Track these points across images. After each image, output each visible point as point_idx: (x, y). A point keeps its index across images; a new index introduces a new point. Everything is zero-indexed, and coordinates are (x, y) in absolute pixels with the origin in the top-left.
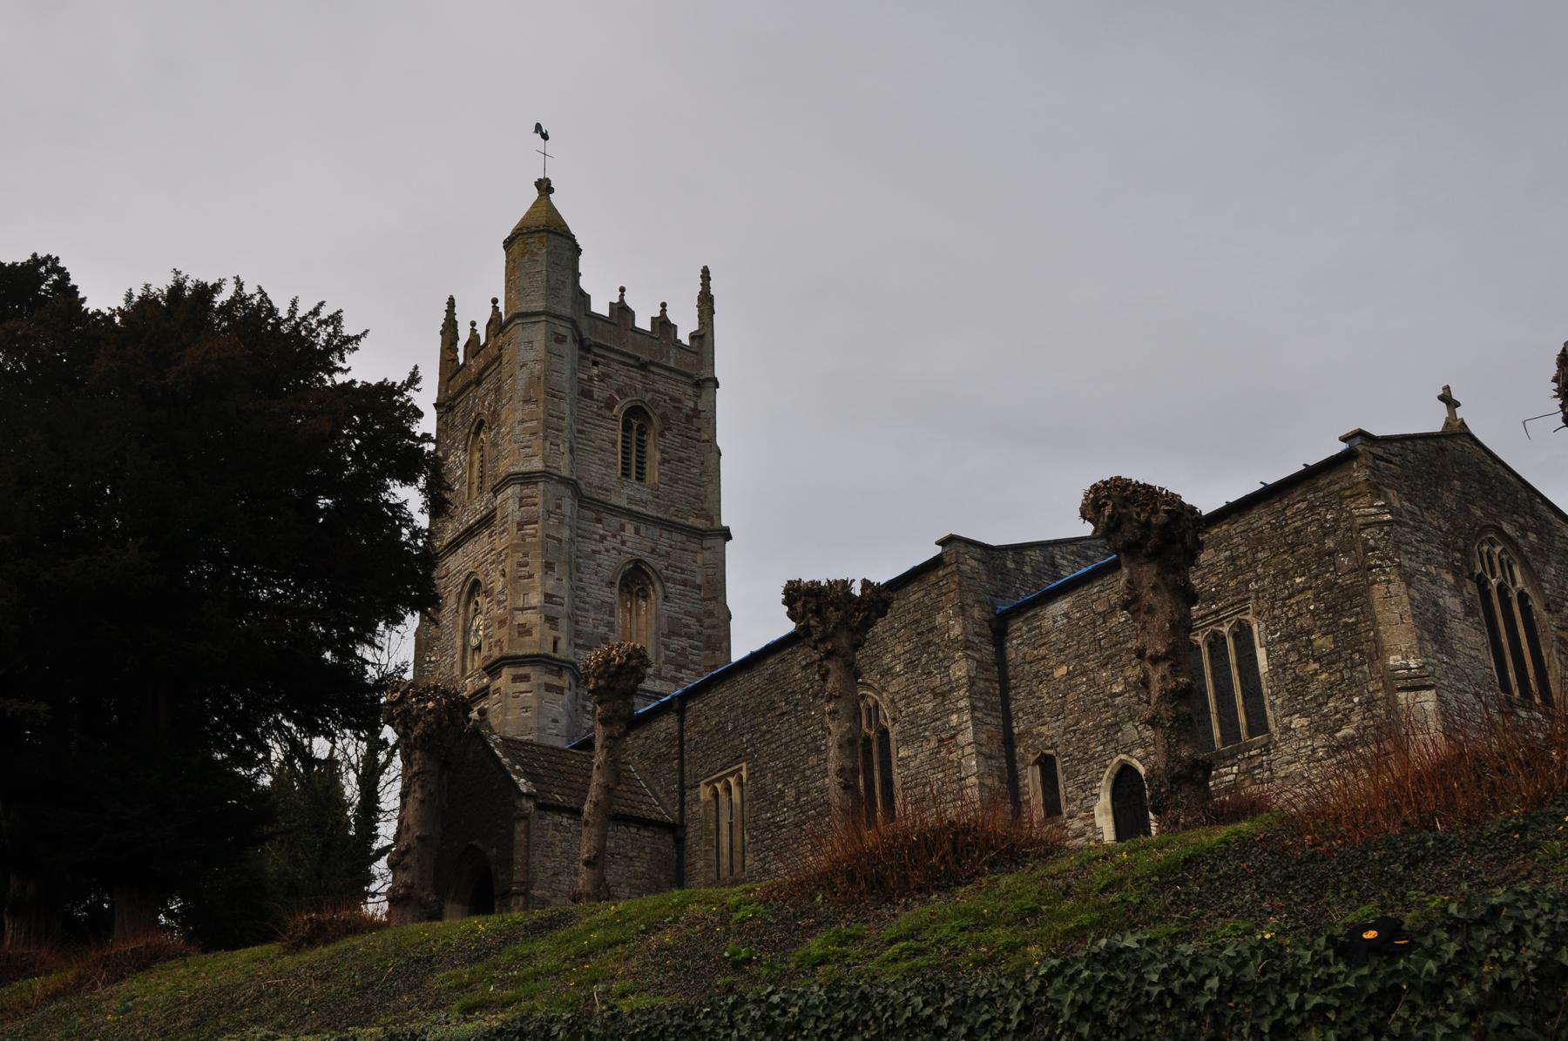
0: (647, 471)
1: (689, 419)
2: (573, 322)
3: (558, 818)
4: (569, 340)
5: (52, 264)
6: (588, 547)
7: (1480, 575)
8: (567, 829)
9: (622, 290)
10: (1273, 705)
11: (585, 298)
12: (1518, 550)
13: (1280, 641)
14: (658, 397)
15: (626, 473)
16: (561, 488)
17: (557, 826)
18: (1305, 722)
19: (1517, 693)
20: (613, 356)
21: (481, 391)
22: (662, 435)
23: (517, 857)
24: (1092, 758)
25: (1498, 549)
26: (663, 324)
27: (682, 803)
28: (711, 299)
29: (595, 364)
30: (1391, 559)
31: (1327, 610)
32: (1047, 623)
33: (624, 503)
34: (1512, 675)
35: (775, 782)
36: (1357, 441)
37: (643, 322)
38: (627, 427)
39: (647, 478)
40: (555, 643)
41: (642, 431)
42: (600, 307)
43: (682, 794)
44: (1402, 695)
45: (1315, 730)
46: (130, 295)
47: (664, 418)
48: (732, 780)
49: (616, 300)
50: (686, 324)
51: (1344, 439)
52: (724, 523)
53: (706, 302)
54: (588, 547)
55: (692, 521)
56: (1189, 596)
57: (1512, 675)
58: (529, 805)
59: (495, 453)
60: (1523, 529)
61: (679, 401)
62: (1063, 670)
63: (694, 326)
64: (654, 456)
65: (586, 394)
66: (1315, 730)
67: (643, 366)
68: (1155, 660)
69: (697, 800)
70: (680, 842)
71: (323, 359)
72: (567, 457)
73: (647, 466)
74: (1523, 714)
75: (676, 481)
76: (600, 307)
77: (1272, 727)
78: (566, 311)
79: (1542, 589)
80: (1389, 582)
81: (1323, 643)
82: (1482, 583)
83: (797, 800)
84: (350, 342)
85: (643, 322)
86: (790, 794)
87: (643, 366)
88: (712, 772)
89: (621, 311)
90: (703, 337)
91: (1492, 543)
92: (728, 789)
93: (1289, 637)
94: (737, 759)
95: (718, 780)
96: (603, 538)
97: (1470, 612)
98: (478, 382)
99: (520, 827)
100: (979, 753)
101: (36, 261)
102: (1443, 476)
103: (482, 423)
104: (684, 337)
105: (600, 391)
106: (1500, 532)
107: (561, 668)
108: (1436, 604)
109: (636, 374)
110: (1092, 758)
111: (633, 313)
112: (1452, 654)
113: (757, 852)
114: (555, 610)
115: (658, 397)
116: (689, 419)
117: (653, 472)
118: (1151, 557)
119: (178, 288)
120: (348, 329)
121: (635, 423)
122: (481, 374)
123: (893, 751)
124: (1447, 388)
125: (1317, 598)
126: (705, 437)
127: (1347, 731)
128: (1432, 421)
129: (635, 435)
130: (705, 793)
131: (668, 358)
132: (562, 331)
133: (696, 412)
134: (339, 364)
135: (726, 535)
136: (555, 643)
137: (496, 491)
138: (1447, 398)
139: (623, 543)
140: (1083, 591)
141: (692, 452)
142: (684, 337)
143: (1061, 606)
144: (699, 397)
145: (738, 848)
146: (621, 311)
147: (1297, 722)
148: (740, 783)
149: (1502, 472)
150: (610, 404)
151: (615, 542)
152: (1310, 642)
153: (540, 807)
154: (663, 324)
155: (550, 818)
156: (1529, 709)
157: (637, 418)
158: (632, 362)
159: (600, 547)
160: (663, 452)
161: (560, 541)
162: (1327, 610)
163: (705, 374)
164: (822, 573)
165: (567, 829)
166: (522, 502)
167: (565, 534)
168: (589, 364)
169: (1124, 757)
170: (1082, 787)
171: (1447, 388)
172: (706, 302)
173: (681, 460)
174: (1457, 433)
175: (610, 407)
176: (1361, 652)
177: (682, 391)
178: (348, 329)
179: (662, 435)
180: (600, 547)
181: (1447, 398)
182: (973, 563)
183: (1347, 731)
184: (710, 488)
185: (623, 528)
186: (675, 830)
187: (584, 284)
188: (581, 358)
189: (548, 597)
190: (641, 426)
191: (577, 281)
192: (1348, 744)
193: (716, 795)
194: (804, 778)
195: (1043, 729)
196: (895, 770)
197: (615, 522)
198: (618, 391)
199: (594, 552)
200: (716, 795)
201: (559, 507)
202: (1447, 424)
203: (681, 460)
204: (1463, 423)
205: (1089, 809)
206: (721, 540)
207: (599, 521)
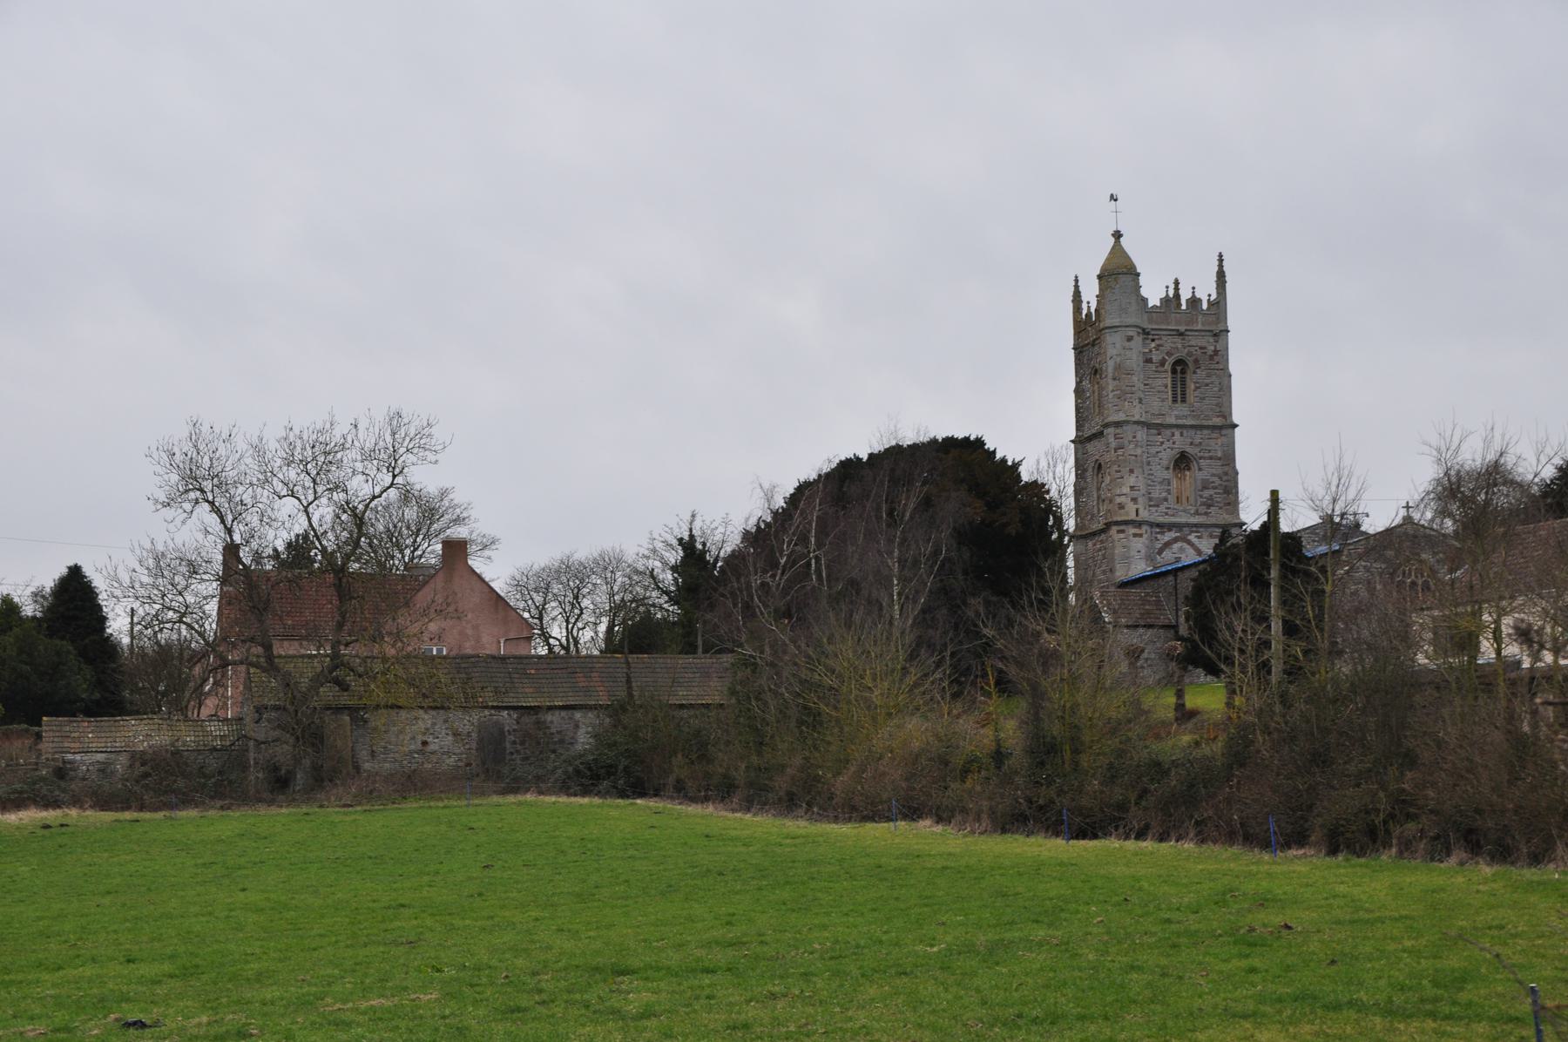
0: (131, 1030)
1: (1211, 357)
11: (1145, 300)
15: (1175, 401)
38: (1174, 371)
65: (1149, 361)
76: (1154, 300)
105: (1156, 357)
109: (1178, 340)
116: (1211, 357)
164: (1233, 321)
187: (1144, 292)
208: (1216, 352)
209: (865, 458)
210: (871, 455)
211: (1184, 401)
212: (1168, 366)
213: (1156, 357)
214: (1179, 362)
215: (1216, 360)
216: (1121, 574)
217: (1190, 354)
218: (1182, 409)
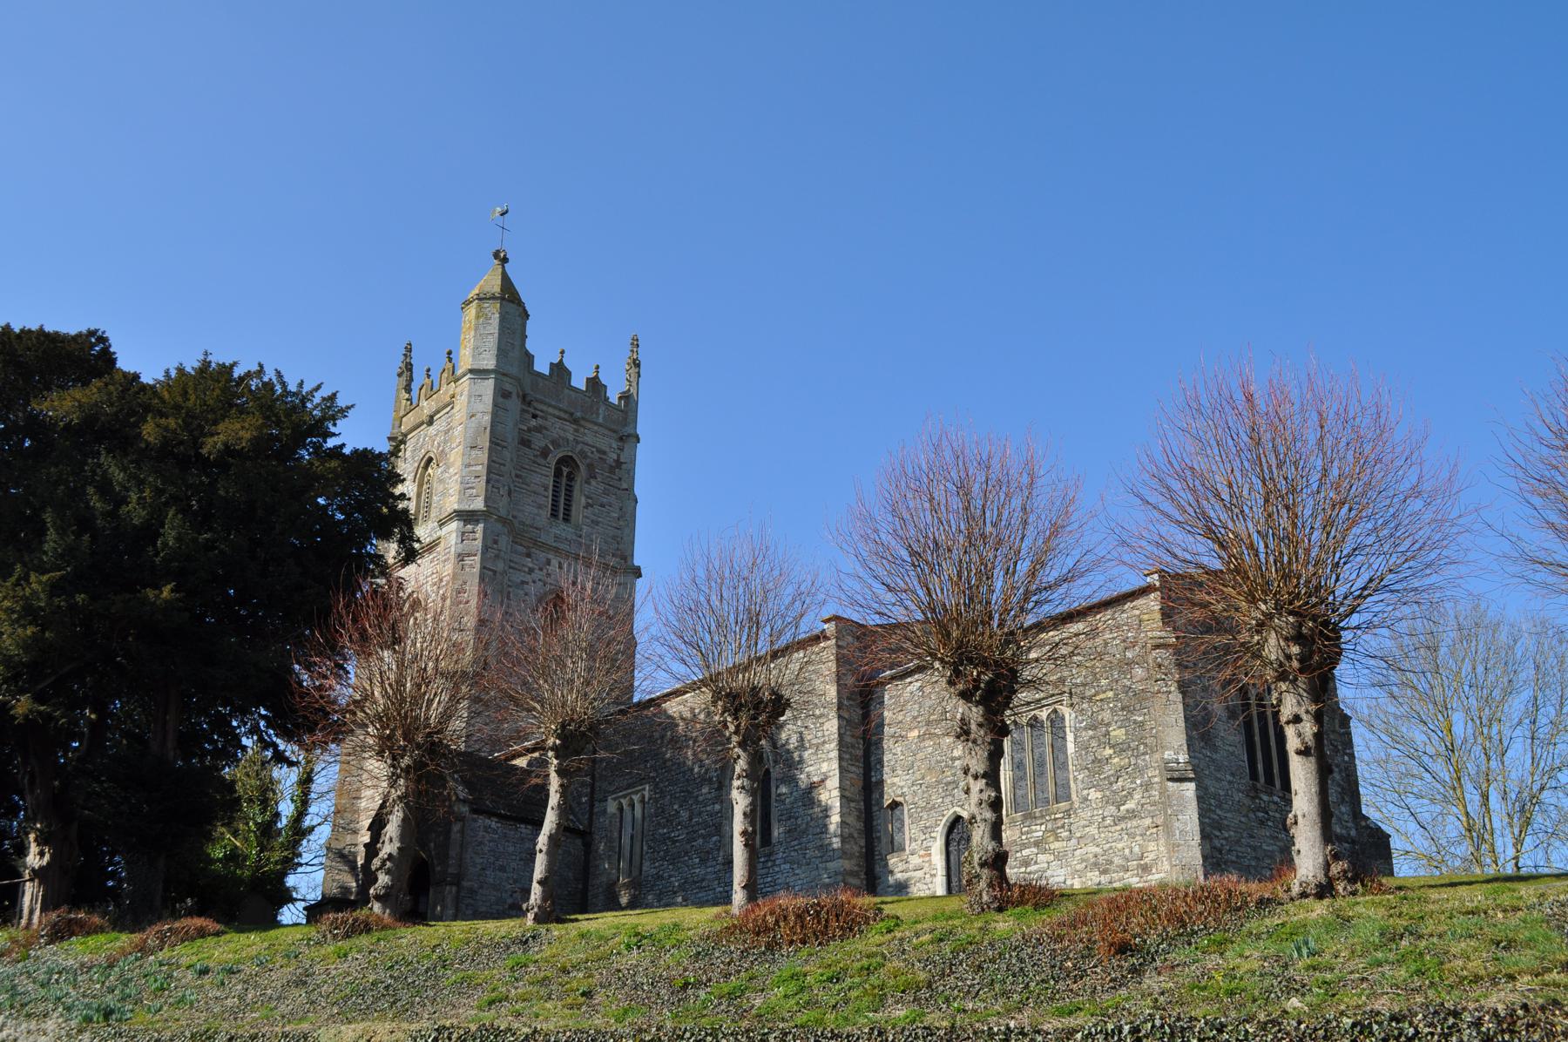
0: (573, 513)
1: (612, 470)
2: (518, 380)
4: (514, 396)
5: (103, 340)
6: (517, 577)
8: (495, 832)
9: (562, 352)
10: (1076, 779)
11: (529, 358)
13: (1085, 729)
15: (554, 514)
17: (487, 829)
18: (1099, 795)
19: (1262, 780)
20: (551, 410)
21: (432, 430)
22: (588, 482)
23: (452, 853)
24: (933, 807)
27: (591, 814)
29: (535, 416)
31: (1123, 709)
32: (907, 695)
33: (551, 542)
34: (1260, 767)
35: (672, 804)
37: (579, 382)
38: (558, 473)
39: (573, 519)
41: (571, 478)
42: (542, 366)
43: (592, 806)
45: (1107, 801)
46: (167, 372)
47: (590, 467)
48: (636, 798)
49: (556, 361)
52: (636, 563)
54: (517, 577)
56: (1004, 731)
57: (1260, 767)
58: (465, 809)
59: (441, 488)
61: (604, 453)
62: (915, 733)
64: (579, 500)
65: (525, 443)
66: (1107, 801)
67: (576, 421)
68: (976, 777)
69: (605, 811)
70: (588, 847)
71: (320, 428)
72: (506, 499)
73: (574, 508)
74: (1265, 798)
75: (597, 523)
76: (542, 366)
77: (1074, 796)
78: (514, 371)
81: (1118, 734)
83: (691, 819)
84: (343, 412)
85: (579, 382)
86: (684, 815)
88: (619, 789)
89: (559, 370)
92: (633, 806)
93: (1093, 727)
94: (642, 781)
95: (624, 797)
96: (531, 571)
97: (1232, 714)
98: (430, 422)
99: (456, 828)
100: (842, 797)
101: (92, 333)
103: (430, 460)
104: (613, 397)
105: (539, 441)
109: (570, 428)
110: (933, 807)
111: (569, 374)
112: (1215, 749)
113: (653, 860)
116: (612, 470)
117: (578, 512)
118: (978, 703)
119: (206, 364)
120: (341, 402)
121: (565, 470)
122: (432, 417)
123: (773, 789)
125: (1116, 698)
126: (625, 486)
127: (1130, 805)
129: (564, 480)
130: (612, 807)
132: (508, 387)
133: (619, 463)
134: (333, 429)
135: (638, 573)
137: (442, 524)
139: (548, 575)
141: (612, 499)
144: (622, 450)
145: (637, 858)
146: (559, 370)
147: (1094, 795)
148: (642, 801)
150: (545, 453)
152: (1108, 733)
155: (482, 821)
156: (1271, 794)
157: (566, 469)
158: (562, 415)
159: (528, 578)
160: (588, 497)
161: (495, 572)
162: (1123, 709)
163: (628, 430)
164: (644, 425)
165: (495, 832)
166: (463, 536)
167: (500, 566)
168: (529, 416)
169: (958, 809)
170: (925, 830)
173: (602, 506)
176: (1146, 745)
177: (607, 443)
178: (341, 402)
179: (588, 482)
180: (528, 578)
183: (1130, 805)
184: (627, 531)
185: (548, 562)
187: (530, 346)
188: (523, 411)
190: (569, 474)
192: (1132, 815)
193: (621, 809)
194: (697, 802)
195: (896, 780)
196: (774, 804)
198: (553, 442)
199: (523, 582)
200: (621, 809)
201: (496, 542)
203: (602, 506)
205: (928, 848)
207: (528, 555)
208: (619, 463)
209: (17, 330)
210: (22, 331)
211: (567, 519)
212: (552, 460)
213: (539, 441)
214: (566, 461)
215: (619, 476)
216: (941, 890)
217: (583, 454)
218: (561, 529)
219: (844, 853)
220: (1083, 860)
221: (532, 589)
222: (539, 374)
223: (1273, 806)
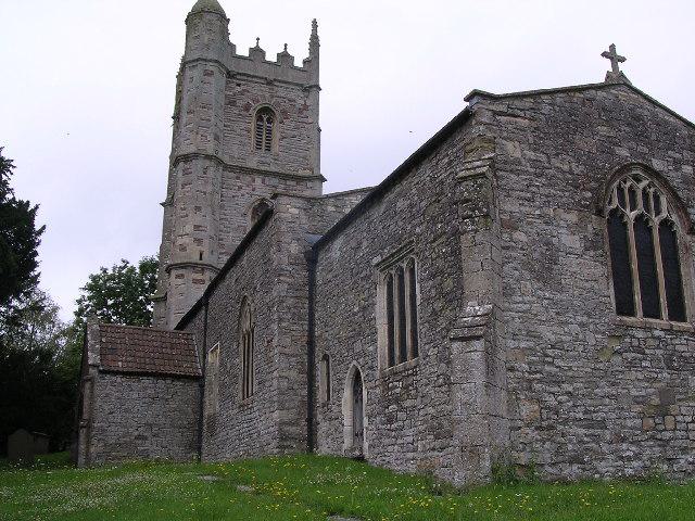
3: (114, 378)
7: (614, 212)
9: (258, 39)
11: (233, 47)
12: (665, 183)
14: (280, 100)
16: (207, 163)
25: (645, 183)
26: (285, 57)
28: (317, 38)
30: (480, 210)
36: (475, 100)
37: (271, 57)
38: (260, 119)
40: (201, 255)
44: (456, 345)
50: (300, 55)
51: (466, 100)
53: (314, 43)
55: (301, 173)
60: (677, 163)
63: (306, 55)
64: (276, 135)
67: (270, 83)
79: (687, 214)
80: (476, 231)
82: (616, 218)
85: (271, 57)
87: (270, 83)
89: (257, 52)
90: (313, 61)
91: (637, 179)
99: (88, 385)
102: (598, 126)
104: (298, 63)
106: (648, 169)
107: (203, 269)
108: (548, 244)
109: (266, 88)
114: (201, 235)
115: (280, 100)
124: (612, 47)
128: (597, 73)
131: (287, 76)
133: (306, 107)
136: (201, 255)
138: (611, 55)
140: (350, 230)
142: (298, 63)
143: (338, 243)
146: (257, 52)
149: (661, 114)
150: (247, 107)
151: (249, 190)
153: (100, 372)
154: (285, 57)
168: (233, 85)
171: (612, 47)
172: (314, 43)
174: (616, 81)
175: (247, 110)
177: (296, 94)
181: (611, 55)
182: (296, 211)
186: (198, 379)
187: (232, 39)
189: (197, 227)
191: (225, 33)
197: (248, 178)
202: (609, 76)
204: (622, 75)
206: (317, 182)
207: (238, 178)
208: (306, 107)
211: (268, 149)
219: (582, 481)
220: (426, 422)
221: (241, 201)
222: (269, 63)
223: (651, 342)
